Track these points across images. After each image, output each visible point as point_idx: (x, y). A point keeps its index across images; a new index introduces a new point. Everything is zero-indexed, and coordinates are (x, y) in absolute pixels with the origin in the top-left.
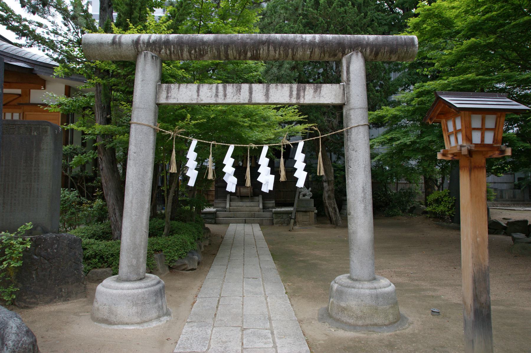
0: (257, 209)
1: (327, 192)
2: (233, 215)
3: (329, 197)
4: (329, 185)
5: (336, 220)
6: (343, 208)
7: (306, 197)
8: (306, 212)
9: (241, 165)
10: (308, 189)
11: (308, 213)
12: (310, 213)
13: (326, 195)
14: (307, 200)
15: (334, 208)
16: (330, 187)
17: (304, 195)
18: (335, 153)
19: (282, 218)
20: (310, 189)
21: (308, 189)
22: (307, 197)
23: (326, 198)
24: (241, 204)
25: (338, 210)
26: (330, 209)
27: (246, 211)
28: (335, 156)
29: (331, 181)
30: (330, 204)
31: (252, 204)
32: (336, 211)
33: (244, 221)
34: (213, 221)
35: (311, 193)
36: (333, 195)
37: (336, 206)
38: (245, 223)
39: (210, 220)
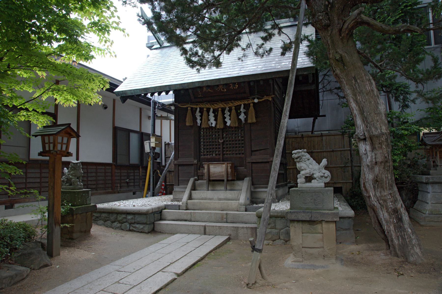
0: (234, 204)
1: (371, 168)
2: (188, 217)
3: (376, 181)
4: (373, 149)
5: (404, 246)
6: (420, 197)
7: (315, 184)
8: (311, 222)
9: (213, 125)
10: (319, 162)
11: (319, 226)
12: (324, 225)
13: (368, 177)
14: (315, 192)
15: (396, 211)
16: (379, 152)
17: (309, 179)
18: (397, 100)
19: (274, 228)
20: (324, 162)
21: (319, 162)
22: (316, 184)
23: (370, 185)
24: (209, 194)
25: (406, 217)
26: (384, 215)
27: (215, 209)
28: (398, 103)
29: (378, 137)
30: (383, 202)
31: (229, 194)
32: (400, 220)
33: (202, 229)
34: (147, 228)
35: (327, 173)
36: (388, 177)
37: (400, 205)
38: (205, 234)
39: (141, 226)
